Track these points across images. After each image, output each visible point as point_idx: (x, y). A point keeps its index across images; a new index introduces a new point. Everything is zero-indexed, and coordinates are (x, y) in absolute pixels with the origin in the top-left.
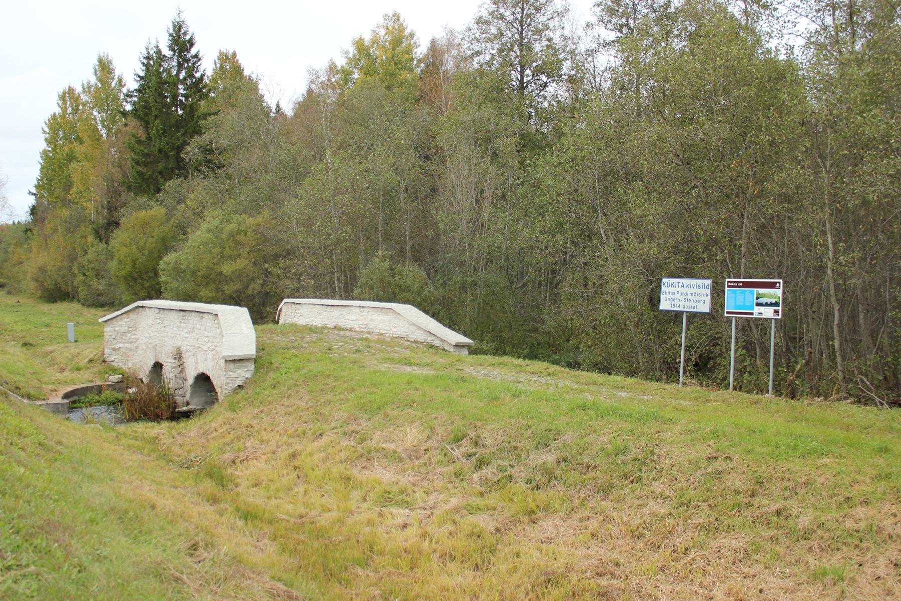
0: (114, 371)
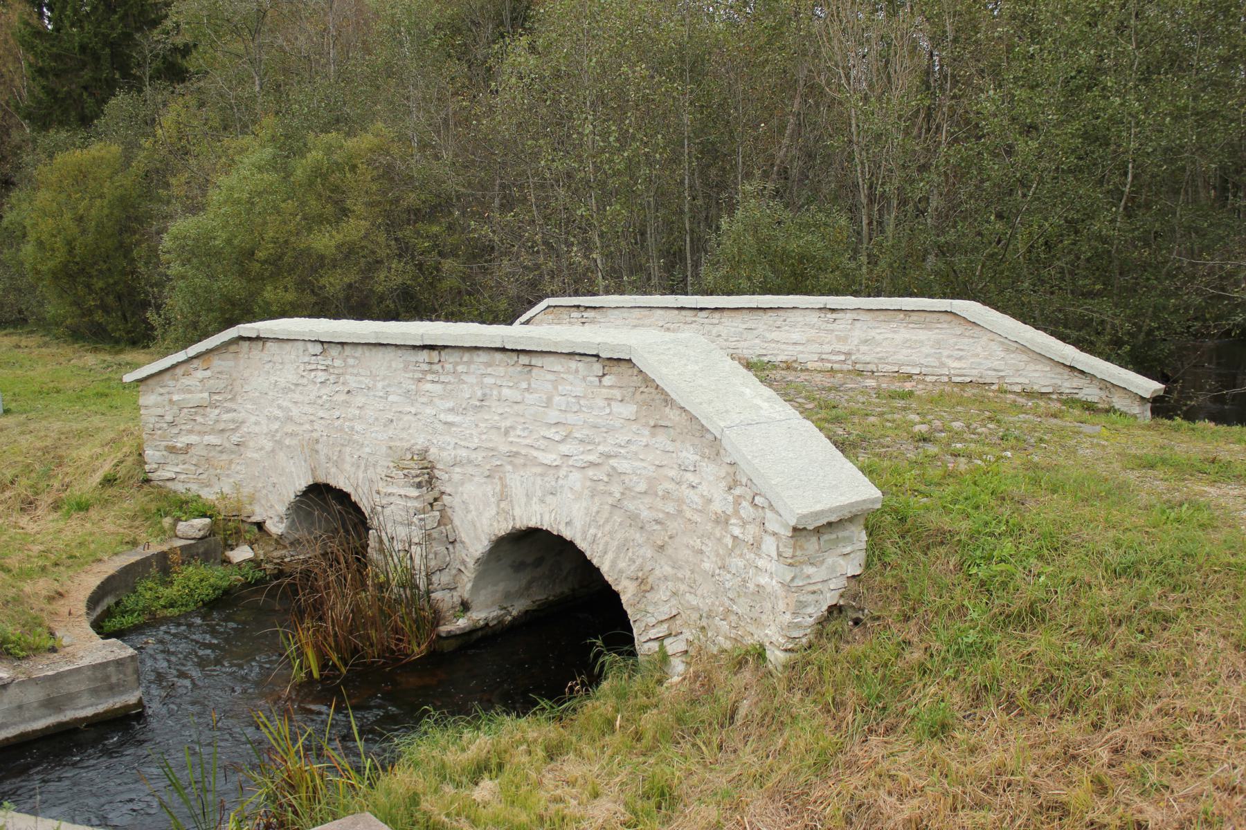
0: (185, 506)
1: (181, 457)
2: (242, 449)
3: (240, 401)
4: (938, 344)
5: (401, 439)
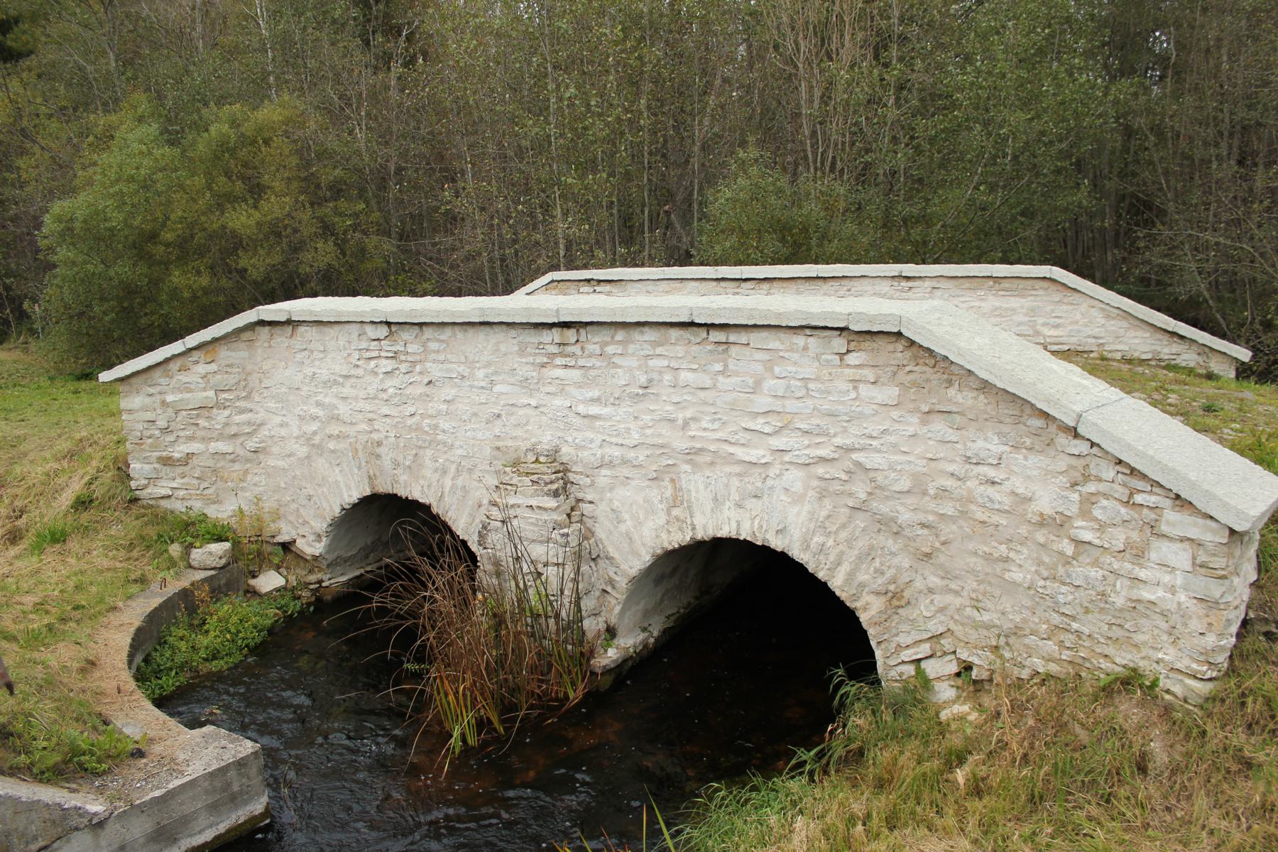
1: (180, 470)
2: (261, 456)
3: (257, 399)
4: (1033, 311)
5: (515, 438)
